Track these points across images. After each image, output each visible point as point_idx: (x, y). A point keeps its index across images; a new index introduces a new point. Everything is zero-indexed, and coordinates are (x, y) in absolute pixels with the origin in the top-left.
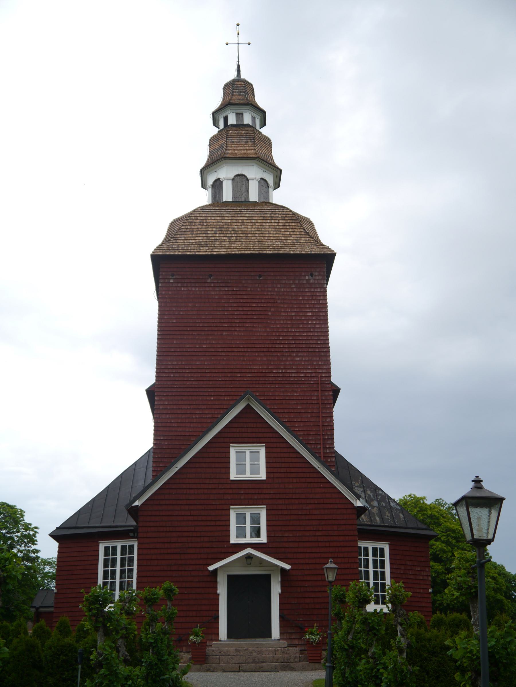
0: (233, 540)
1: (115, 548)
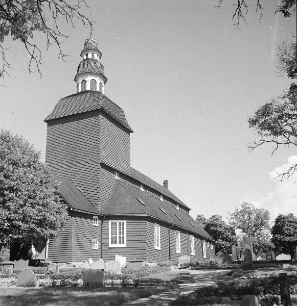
1: (115, 223)
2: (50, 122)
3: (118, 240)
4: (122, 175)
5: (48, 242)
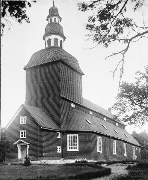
0: (21, 137)
3: (73, 147)
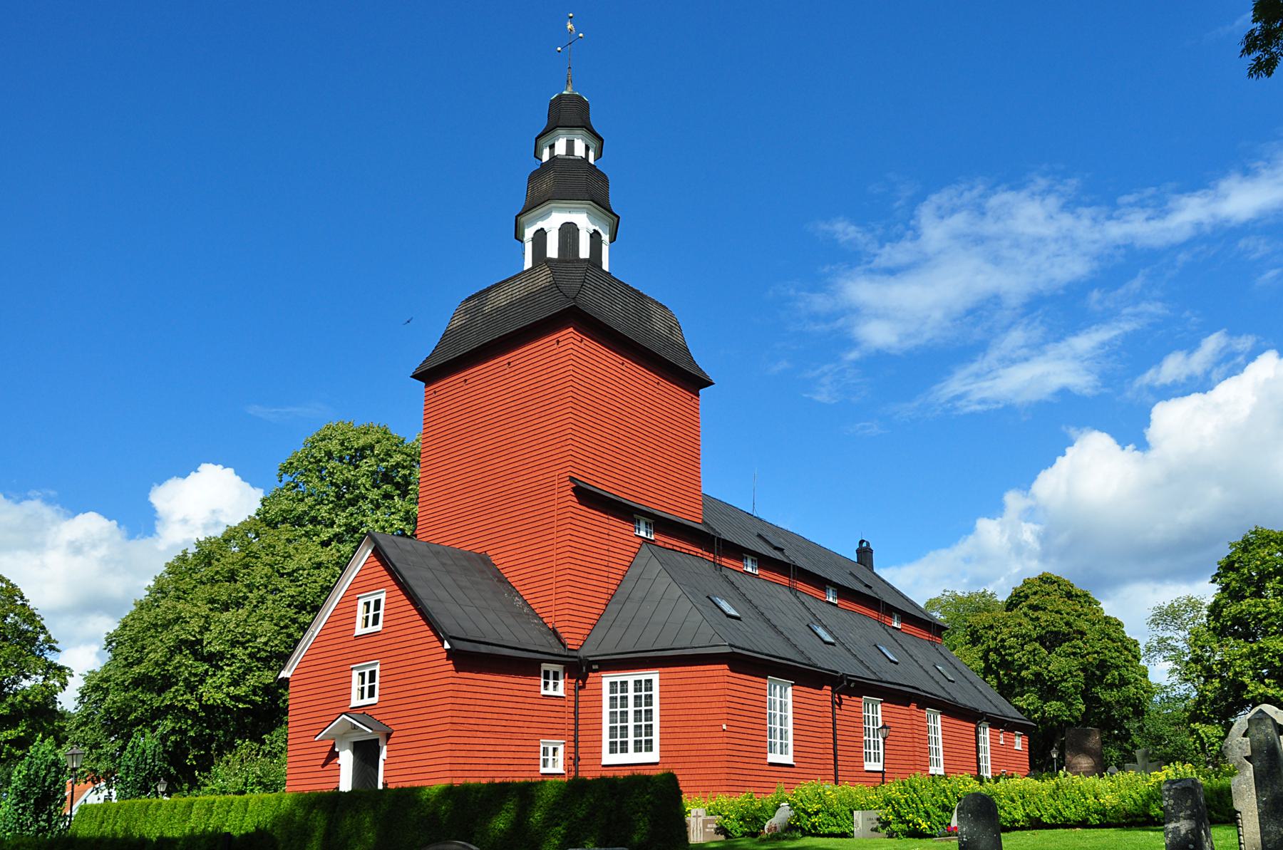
1: (624, 683)
2: (428, 375)
3: (631, 739)
4: (663, 525)
5: (383, 755)
